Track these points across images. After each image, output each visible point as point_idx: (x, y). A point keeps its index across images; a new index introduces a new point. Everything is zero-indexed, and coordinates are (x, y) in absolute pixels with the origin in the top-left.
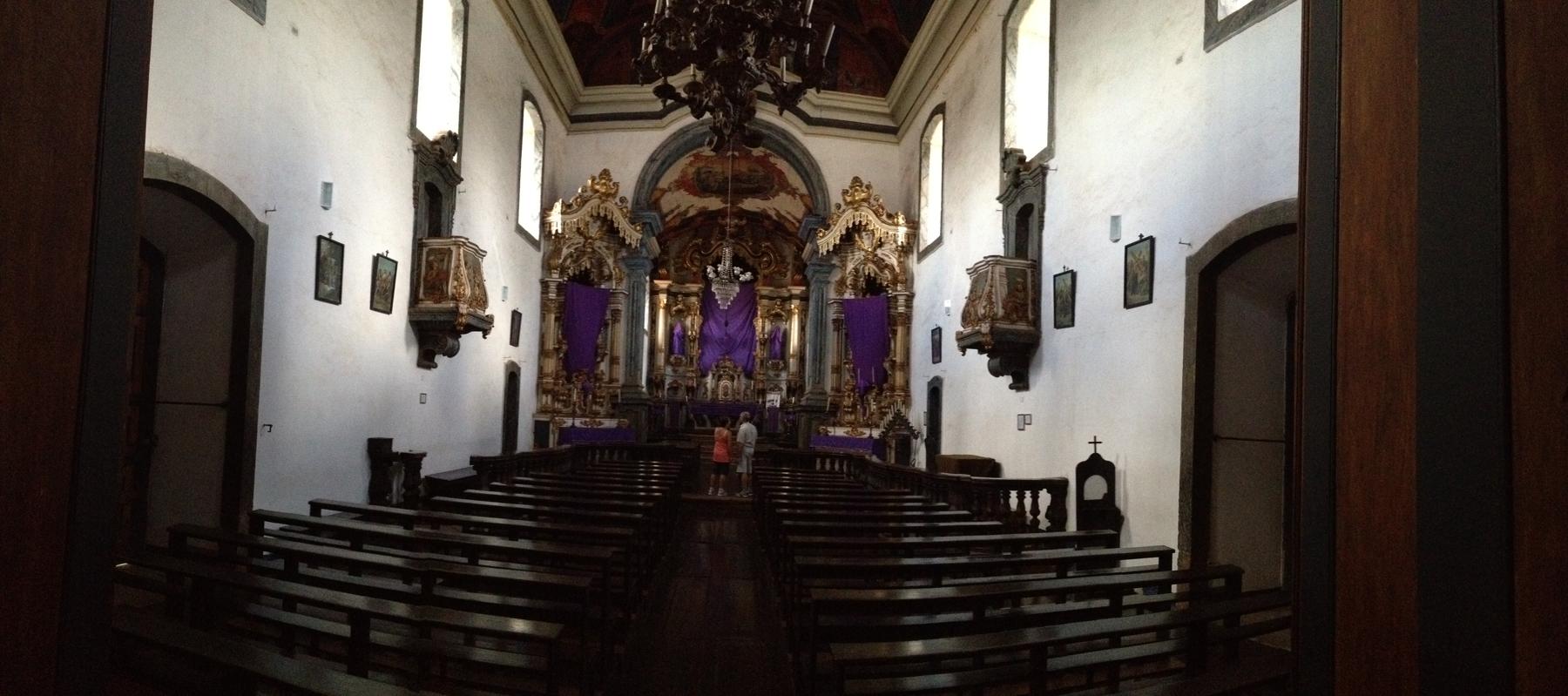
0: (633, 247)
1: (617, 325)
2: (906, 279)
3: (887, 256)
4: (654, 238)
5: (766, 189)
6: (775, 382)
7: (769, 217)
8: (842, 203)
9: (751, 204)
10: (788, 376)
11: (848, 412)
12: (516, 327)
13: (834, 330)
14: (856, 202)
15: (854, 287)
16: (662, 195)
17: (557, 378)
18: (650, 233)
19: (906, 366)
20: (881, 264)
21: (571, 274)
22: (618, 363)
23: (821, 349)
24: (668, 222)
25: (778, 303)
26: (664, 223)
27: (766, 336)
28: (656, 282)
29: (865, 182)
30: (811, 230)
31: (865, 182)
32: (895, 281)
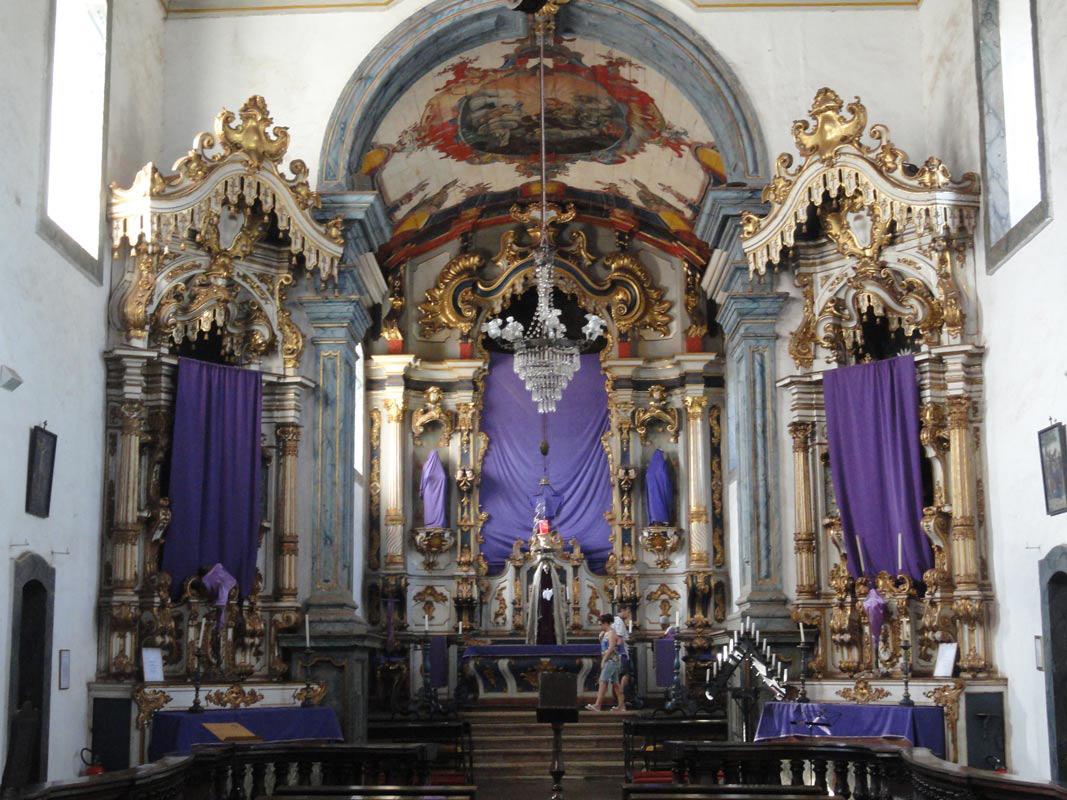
0: (324, 275)
2: (963, 316)
3: (910, 263)
4: (371, 256)
5: (614, 138)
6: (661, 580)
7: (623, 202)
8: (795, 153)
9: (583, 174)
10: (689, 562)
11: (842, 643)
12: (41, 467)
13: (795, 449)
14: (829, 145)
15: (836, 342)
16: (386, 160)
17: (146, 591)
18: (363, 244)
19: (978, 523)
20: (896, 285)
21: (178, 340)
22: (295, 552)
23: (768, 496)
24: (402, 221)
25: (656, 395)
26: (395, 226)
27: (632, 474)
29: (848, 100)
30: (726, 218)
31: (848, 100)
32: (935, 322)
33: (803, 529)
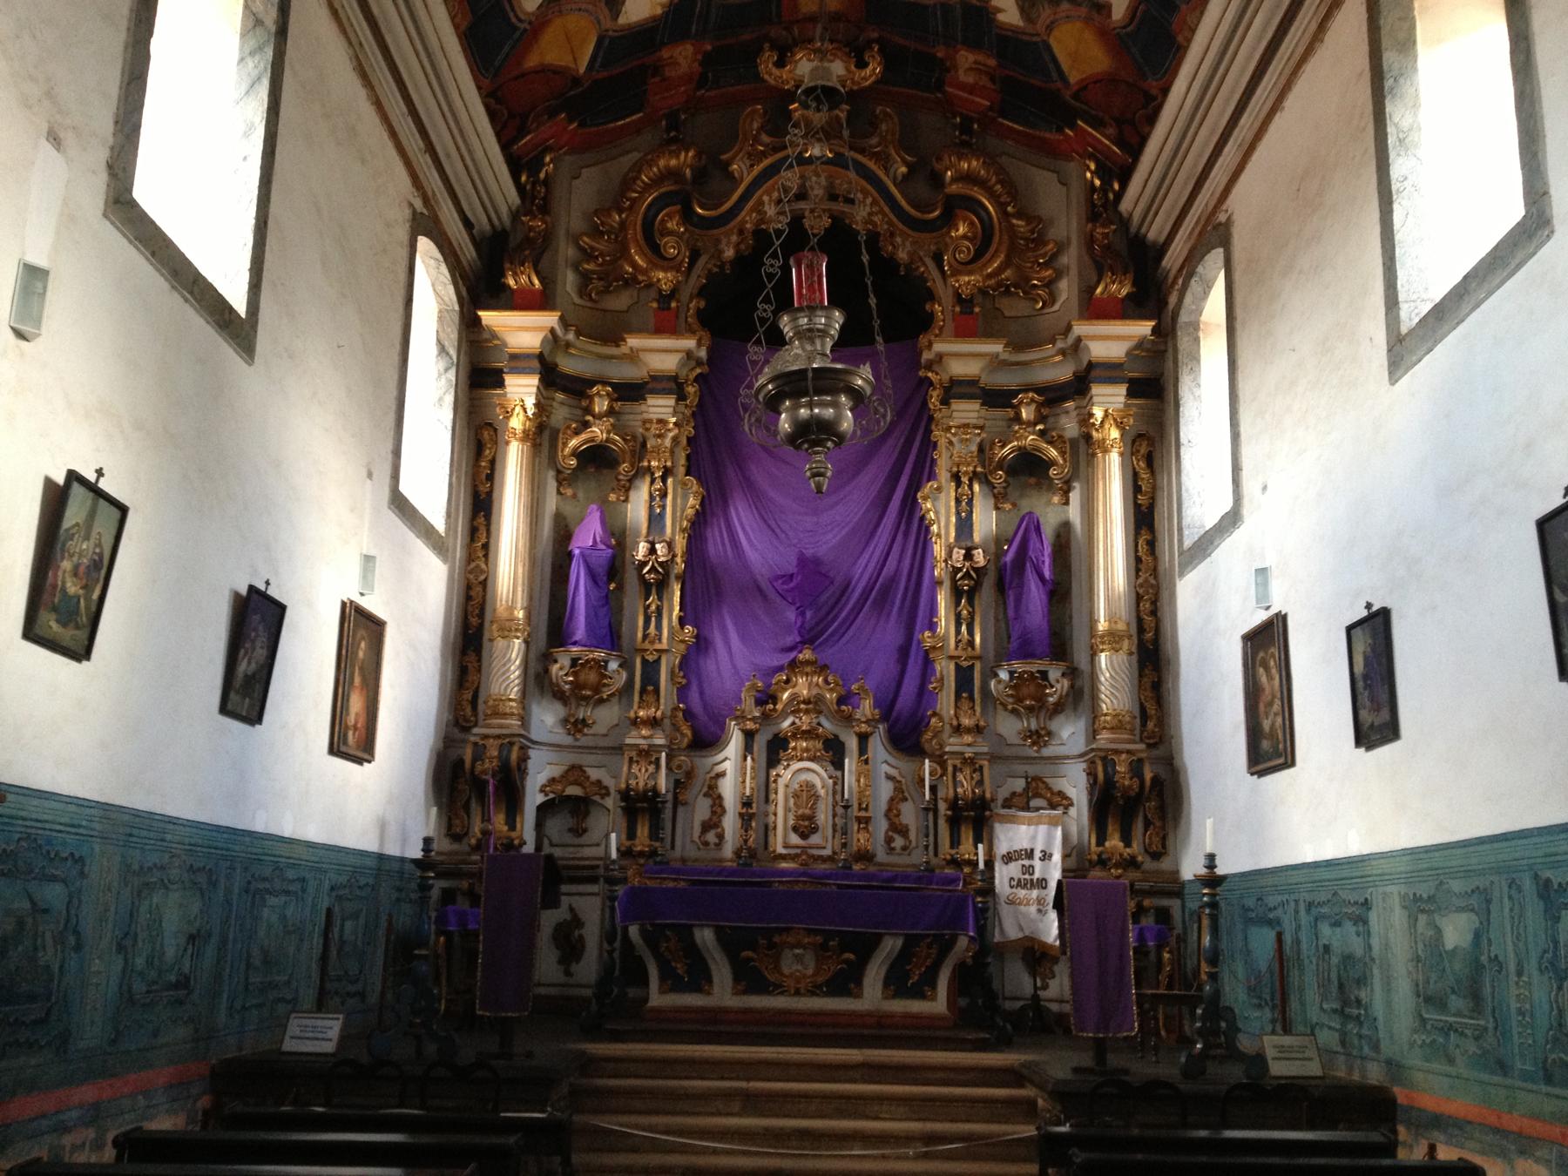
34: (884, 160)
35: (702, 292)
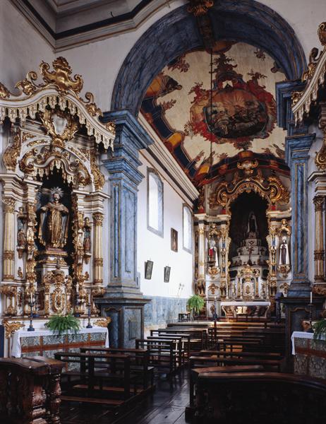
1: (99, 228)
23: (303, 234)
25: (284, 222)
28: (196, 215)
33: (319, 248)
34: (259, 180)
35: (229, 206)
